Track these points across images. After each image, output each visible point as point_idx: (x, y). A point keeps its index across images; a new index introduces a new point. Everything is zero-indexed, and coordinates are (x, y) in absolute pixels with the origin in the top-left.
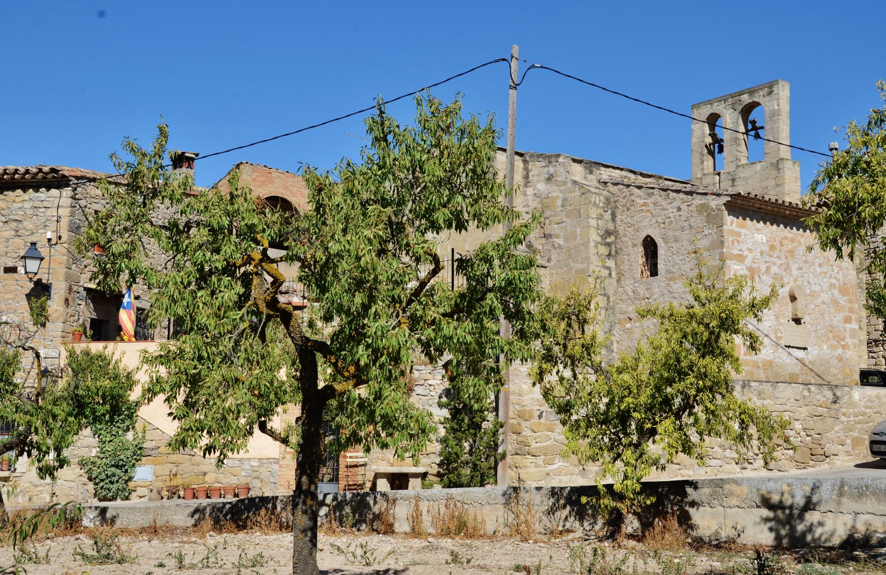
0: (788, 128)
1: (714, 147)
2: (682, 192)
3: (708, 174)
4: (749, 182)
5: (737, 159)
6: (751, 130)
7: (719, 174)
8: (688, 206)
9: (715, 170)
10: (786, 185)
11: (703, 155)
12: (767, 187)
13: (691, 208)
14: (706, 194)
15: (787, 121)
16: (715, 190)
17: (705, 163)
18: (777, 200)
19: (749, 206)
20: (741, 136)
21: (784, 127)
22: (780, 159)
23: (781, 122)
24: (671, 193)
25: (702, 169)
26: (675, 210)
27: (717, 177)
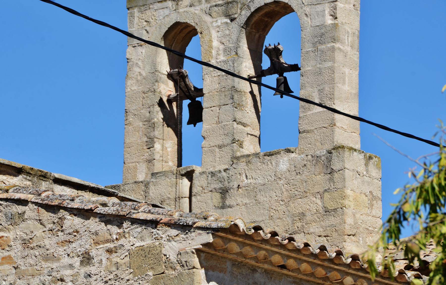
0: (355, 74)
1: (180, 107)
2: (96, 215)
3: (164, 174)
4: (261, 198)
5: (234, 141)
6: (270, 72)
7: (189, 175)
8: (109, 251)
9: (180, 164)
10: (349, 211)
11: (153, 126)
12: (303, 214)
13: (115, 258)
14: (154, 224)
15: (354, 55)
16: (176, 216)
17: (157, 146)
18: (323, 248)
19: (256, 259)
20: (245, 86)
21: (347, 71)
22: (336, 148)
23: (339, 56)
24: (68, 216)
25: (150, 161)
26: (76, 261)
27: (186, 182)
